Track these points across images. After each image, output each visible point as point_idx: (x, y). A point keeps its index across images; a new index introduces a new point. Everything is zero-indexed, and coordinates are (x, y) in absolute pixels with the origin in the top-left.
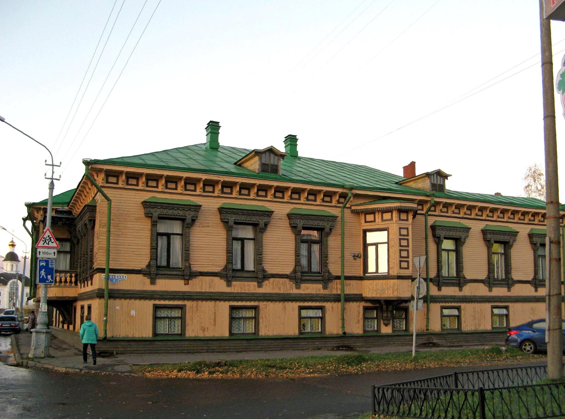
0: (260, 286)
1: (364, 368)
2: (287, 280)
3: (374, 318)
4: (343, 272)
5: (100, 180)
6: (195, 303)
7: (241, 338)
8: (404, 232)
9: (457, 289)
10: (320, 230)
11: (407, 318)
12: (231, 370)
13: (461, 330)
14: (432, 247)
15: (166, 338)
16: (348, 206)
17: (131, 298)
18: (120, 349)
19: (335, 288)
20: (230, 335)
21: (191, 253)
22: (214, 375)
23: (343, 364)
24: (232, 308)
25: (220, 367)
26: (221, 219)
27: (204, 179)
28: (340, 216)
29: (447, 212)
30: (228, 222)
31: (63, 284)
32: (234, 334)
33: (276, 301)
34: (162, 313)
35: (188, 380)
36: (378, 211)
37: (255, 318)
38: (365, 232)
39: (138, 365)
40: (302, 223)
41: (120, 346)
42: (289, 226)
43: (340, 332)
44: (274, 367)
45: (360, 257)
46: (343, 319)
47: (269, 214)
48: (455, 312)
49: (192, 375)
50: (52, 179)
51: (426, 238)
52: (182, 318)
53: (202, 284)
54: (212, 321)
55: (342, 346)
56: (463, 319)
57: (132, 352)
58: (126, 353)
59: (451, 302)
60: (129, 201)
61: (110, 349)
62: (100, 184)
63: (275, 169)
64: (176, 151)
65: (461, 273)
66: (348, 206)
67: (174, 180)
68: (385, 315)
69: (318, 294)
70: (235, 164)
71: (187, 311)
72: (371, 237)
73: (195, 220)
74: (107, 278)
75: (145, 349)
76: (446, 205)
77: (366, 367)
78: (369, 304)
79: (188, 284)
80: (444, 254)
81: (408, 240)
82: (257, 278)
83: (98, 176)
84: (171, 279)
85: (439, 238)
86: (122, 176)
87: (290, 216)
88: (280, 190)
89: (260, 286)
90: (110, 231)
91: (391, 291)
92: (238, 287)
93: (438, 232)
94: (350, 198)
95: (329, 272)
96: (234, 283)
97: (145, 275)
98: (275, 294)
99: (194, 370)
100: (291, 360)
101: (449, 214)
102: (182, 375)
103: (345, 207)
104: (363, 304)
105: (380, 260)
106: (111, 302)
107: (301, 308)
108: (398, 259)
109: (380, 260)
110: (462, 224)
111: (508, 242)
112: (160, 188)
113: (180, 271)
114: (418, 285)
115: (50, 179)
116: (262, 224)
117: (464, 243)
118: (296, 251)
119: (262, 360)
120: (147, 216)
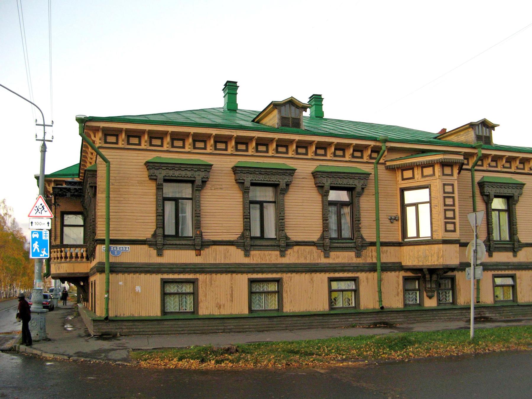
0: (283, 255)
1: (411, 354)
2: (314, 248)
3: (415, 290)
4: (378, 237)
5: (98, 139)
6: (208, 276)
7: (262, 315)
8: (449, 189)
9: (511, 254)
10: (350, 190)
11: (453, 289)
12: (243, 358)
13: (517, 302)
14: (481, 206)
15: (177, 317)
16: (381, 161)
17: (135, 272)
18: (124, 331)
19: (370, 256)
20: (249, 312)
21: (202, 219)
22: (223, 365)
23: (384, 349)
24: (252, 282)
25: (229, 355)
26: (236, 180)
27: (214, 134)
28: (373, 173)
29: (497, 167)
30: (244, 183)
31: (74, 260)
32: (253, 311)
33: (302, 272)
34: (171, 289)
35: (188, 372)
36: (417, 166)
37: (278, 292)
38: (402, 191)
39: (139, 349)
40: (329, 182)
41: (124, 327)
42: (314, 186)
43: (377, 307)
44: (296, 353)
45: (397, 220)
46: (380, 292)
47: (291, 172)
48: (510, 281)
49: (194, 364)
50: (44, 140)
51: (473, 196)
52: (195, 294)
53: (216, 254)
54: (229, 297)
55: (380, 323)
56: (518, 289)
57: (138, 333)
58: (131, 335)
59: (505, 269)
60: (128, 163)
61: (113, 330)
62: (97, 145)
63: (296, 123)
64: (190, 112)
65: (515, 237)
66: (381, 161)
67: (180, 137)
68: (429, 286)
69: (350, 264)
70: (253, 121)
71: (200, 286)
72: (410, 197)
73: (206, 181)
74: (108, 250)
75: (153, 330)
76: (496, 159)
77: (413, 352)
78: (409, 274)
79: (200, 255)
80: (495, 214)
81: (453, 198)
82: (279, 246)
83: (95, 137)
84: (180, 249)
85: (488, 196)
86: (122, 134)
87: (315, 174)
88: (301, 145)
89: (283, 255)
90: (109, 197)
91: (435, 258)
92: (258, 257)
93: (487, 190)
94: (384, 151)
95: (362, 238)
96: (252, 253)
97: (150, 245)
98: (301, 264)
99: (198, 358)
100: (319, 343)
101: (499, 169)
102: (184, 364)
103: (378, 163)
104: (402, 274)
105: (421, 222)
106: (113, 277)
107: (331, 280)
108: (443, 220)
109: (421, 222)
110: (514, 180)
111: (511, 197)
112: (166, 147)
113: (191, 240)
114: (474, 248)
115: (42, 140)
116: (283, 185)
117: (517, 201)
118: (323, 214)
119: (284, 343)
120: (150, 179)
